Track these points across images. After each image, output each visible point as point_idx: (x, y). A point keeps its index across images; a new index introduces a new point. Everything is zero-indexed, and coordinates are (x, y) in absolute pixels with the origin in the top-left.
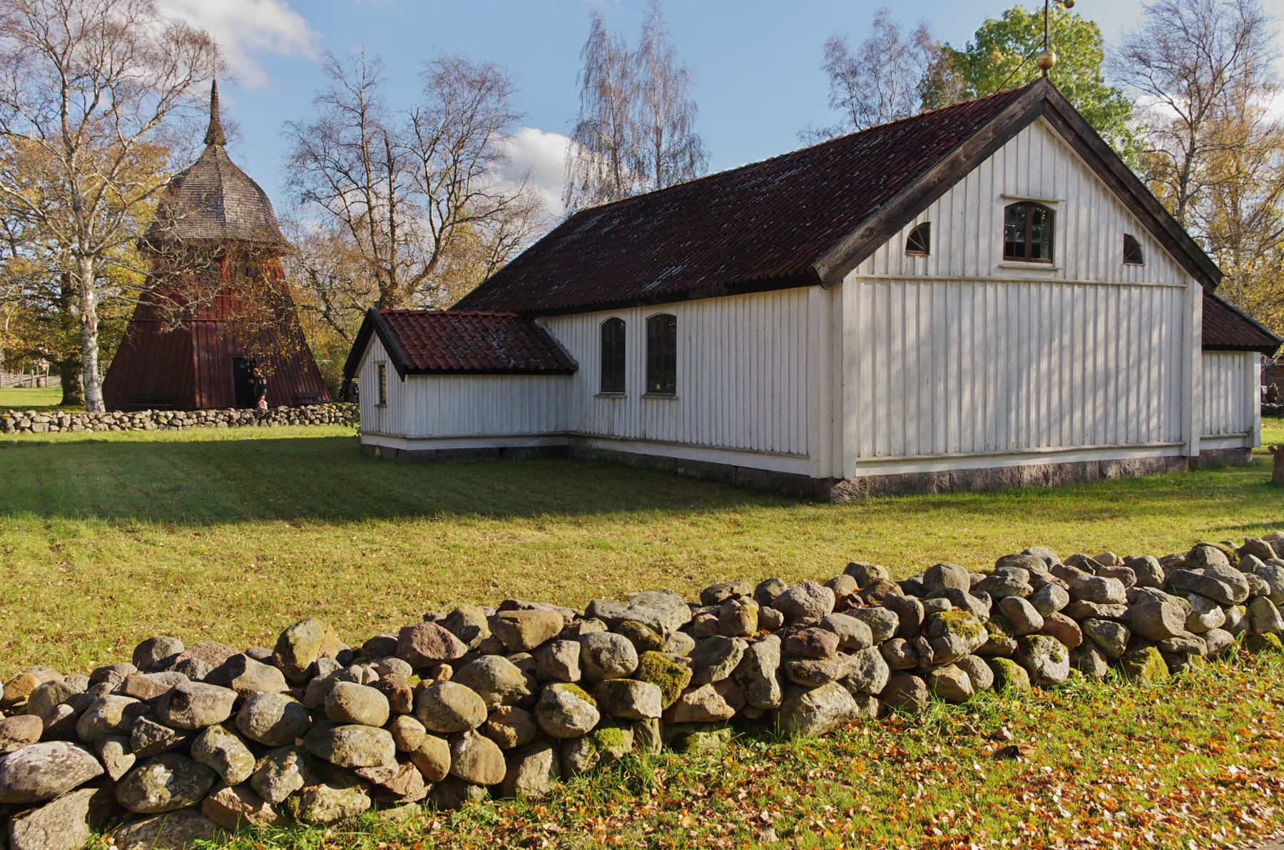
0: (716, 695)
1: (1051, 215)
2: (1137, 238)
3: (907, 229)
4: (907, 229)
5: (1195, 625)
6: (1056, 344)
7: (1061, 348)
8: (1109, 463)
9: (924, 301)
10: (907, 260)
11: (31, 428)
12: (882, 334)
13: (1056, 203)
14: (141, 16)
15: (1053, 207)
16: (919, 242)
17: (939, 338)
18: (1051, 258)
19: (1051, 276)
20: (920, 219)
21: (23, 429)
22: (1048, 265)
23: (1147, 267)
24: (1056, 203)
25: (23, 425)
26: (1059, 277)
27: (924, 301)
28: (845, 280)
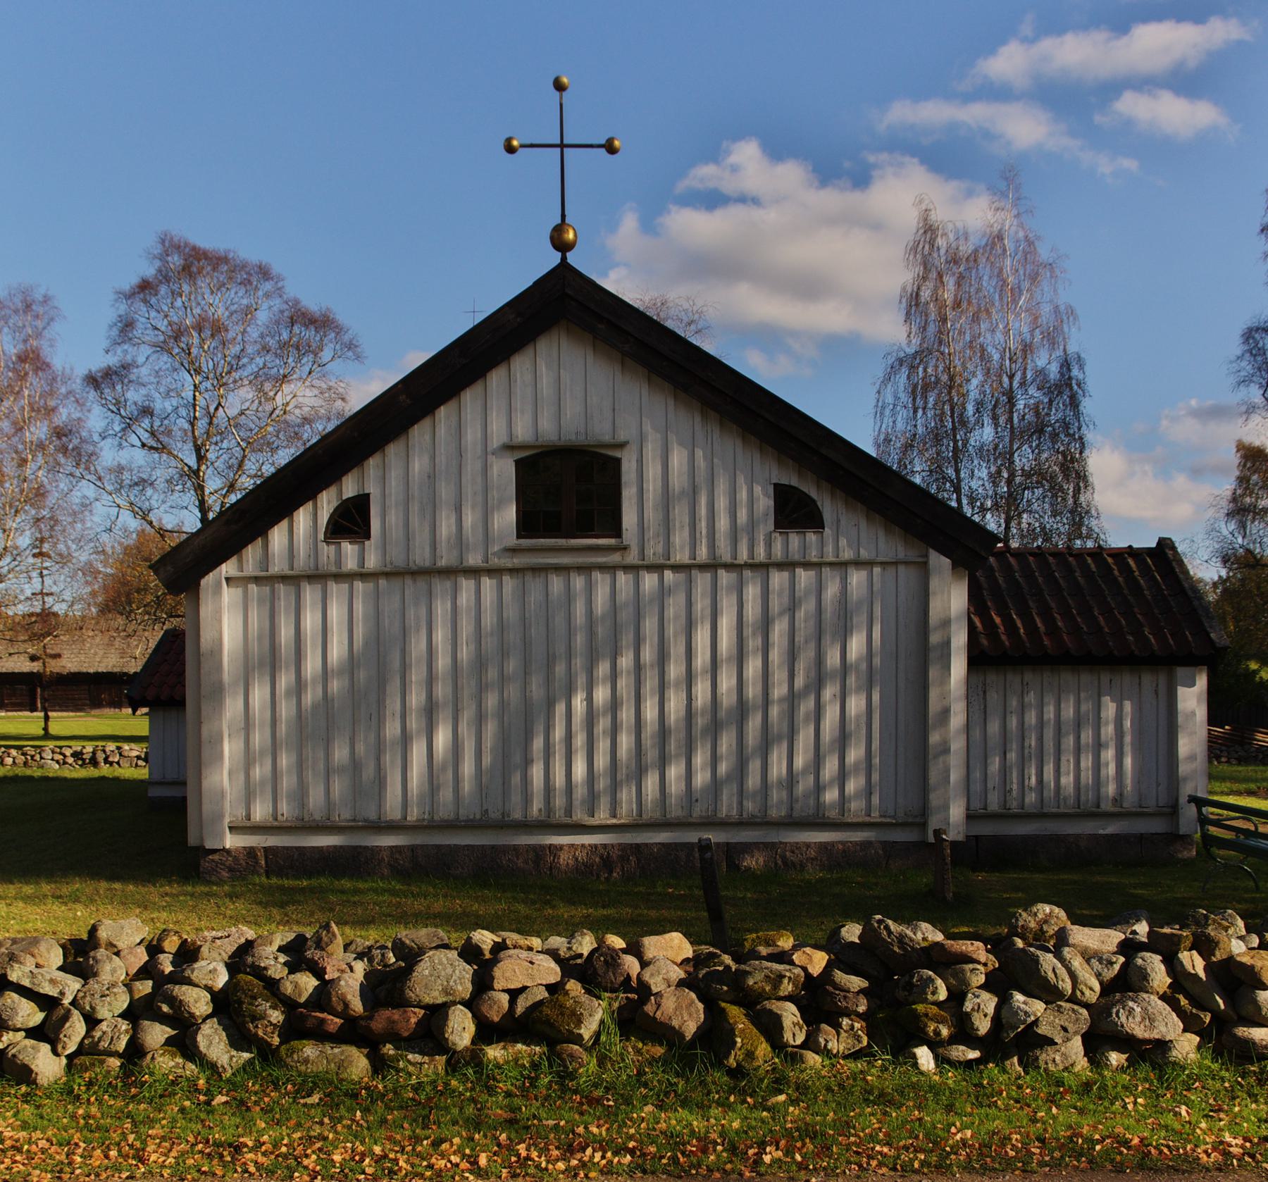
0: (989, 1018)
1: (614, 466)
2: (805, 490)
3: (327, 503)
4: (327, 503)
5: (868, 1164)
6: (625, 661)
7: (638, 667)
8: (747, 848)
9: (336, 612)
10: (327, 551)
11: (118, 763)
12: (267, 658)
13: (621, 446)
14: (279, 400)
15: (617, 454)
16: (351, 522)
17: (377, 665)
18: (617, 531)
19: (615, 558)
20: (349, 487)
21: (111, 764)
22: (612, 541)
23: (827, 531)
24: (621, 446)
25: (111, 759)
26: (632, 557)
27: (336, 612)
28: (203, 582)
